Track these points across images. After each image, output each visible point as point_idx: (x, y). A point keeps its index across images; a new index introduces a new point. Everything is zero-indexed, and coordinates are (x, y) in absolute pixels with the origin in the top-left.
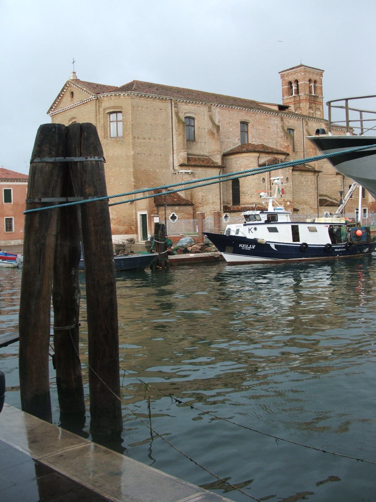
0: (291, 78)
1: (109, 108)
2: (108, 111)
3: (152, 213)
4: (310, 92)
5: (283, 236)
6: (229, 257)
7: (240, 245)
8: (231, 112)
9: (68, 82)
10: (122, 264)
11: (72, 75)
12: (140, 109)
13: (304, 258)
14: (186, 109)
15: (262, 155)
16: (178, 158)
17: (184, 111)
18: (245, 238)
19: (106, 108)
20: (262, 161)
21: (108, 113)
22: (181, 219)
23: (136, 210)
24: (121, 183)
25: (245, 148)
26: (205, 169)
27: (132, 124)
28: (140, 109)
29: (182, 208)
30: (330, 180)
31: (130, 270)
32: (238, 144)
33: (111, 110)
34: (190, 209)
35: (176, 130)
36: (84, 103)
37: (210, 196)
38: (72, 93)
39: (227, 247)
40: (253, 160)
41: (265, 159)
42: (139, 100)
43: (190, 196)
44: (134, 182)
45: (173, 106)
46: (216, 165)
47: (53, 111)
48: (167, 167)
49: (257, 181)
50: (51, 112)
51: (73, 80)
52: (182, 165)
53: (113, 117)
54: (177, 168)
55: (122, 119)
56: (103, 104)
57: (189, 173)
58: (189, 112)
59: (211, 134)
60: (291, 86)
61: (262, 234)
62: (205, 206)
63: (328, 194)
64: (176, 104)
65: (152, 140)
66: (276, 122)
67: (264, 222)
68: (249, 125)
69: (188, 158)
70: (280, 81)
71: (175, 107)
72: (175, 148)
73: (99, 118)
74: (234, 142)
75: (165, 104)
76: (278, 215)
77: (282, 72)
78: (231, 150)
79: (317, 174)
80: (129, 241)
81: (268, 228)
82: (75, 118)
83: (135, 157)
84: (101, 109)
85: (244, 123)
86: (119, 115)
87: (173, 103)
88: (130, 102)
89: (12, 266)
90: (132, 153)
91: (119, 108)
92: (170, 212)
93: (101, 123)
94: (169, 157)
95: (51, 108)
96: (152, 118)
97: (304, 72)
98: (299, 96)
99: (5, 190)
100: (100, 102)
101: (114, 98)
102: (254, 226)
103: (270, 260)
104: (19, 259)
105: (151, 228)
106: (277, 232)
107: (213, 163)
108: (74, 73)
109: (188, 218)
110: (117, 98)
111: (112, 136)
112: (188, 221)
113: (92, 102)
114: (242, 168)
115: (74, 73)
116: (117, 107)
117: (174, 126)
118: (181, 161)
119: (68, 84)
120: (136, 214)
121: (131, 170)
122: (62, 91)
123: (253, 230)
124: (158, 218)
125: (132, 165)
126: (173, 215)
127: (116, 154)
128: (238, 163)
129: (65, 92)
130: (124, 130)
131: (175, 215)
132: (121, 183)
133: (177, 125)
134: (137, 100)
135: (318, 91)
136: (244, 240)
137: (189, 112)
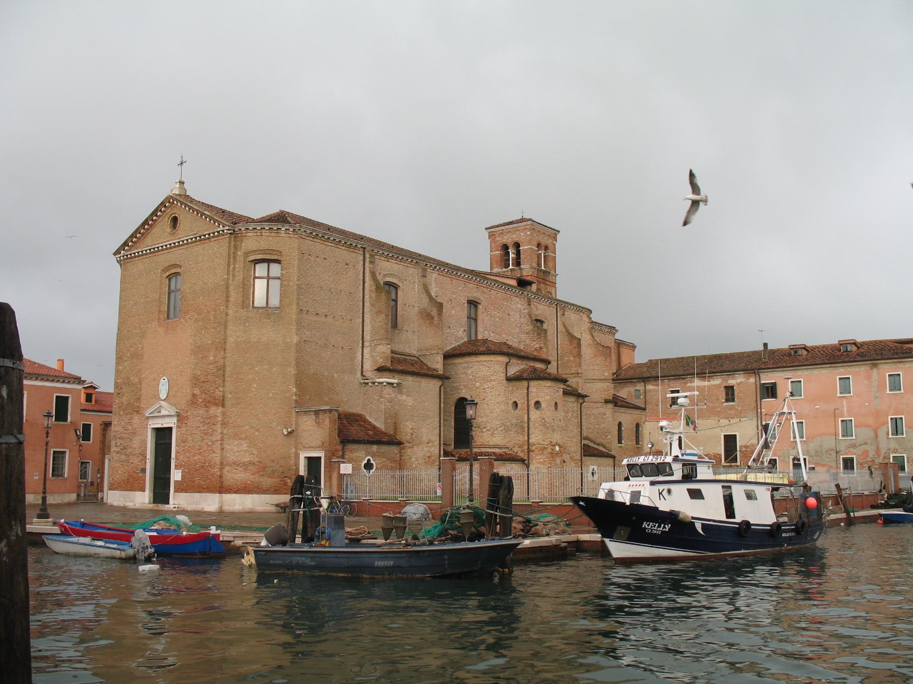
0: (509, 239)
3: (333, 454)
4: (539, 265)
5: (708, 509)
6: (618, 549)
7: (645, 525)
8: (454, 281)
9: (168, 199)
10: (446, 562)
11: (178, 185)
12: (313, 259)
13: (743, 551)
14: (388, 269)
15: (513, 361)
16: (372, 356)
17: (384, 273)
18: (656, 509)
20: (512, 371)
21: (252, 261)
22: (381, 469)
23: (297, 449)
24: (271, 395)
25: (474, 348)
26: (419, 379)
27: (298, 285)
28: (313, 259)
29: (384, 448)
30: (595, 411)
31: (459, 576)
32: (462, 338)
34: (394, 449)
35: (372, 305)
36: (201, 239)
37: (424, 430)
38: (175, 220)
39: (619, 528)
40: (497, 367)
41: (516, 367)
42: (311, 243)
43: (392, 428)
44: (296, 395)
45: (367, 260)
46: (435, 373)
47: (127, 251)
48: (352, 371)
49: (503, 407)
51: (180, 195)
52: (381, 370)
53: (261, 270)
54: (369, 374)
55: (279, 275)
57: (392, 384)
58: (391, 275)
59: (426, 316)
60: (507, 253)
61: (676, 501)
62: (415, 448)
63: (591, 436)
64: (372, 256)
65: (330, 319)
66: (519, 306)
67: (680, 479)
68: (480, 307)
69: (392, 357)
70: (487, 242)
71: (371, 262)
72: (367, 337)
73: (234, 268)
74: (457, 336)
75: (353, 255)
77: (492, 227)
78: (454, 349)
79: (581, 401)
80: (282, 508)
81: (689, 490)
82: (180, 266)
83: (301, 347)
84: (239, 253)
85: (473, 304)
86: (273, 266)
87: (367, 256)
88: (296, 244)
89: (123, 555)
90: (295, 339)
92: (363, 454)
93: (237, 278)
94: (356, 353)
95: (126, 244)
96: (331, 279)
97: (530, 230)
98: (521, 269)
99: (68, 397)
100: (239, 239)
102: (666, 487)
103: (691, 554)
104: (140, 540)
105: (331, 484)
106: (703, 498)
107: (429, 368)
108: (182, 183)
109: (392, 469)
111: (256, 305)
112: (391, 473)
113: (221, 237)
115: (182, 183)
117: (367, 297)
118: (381, 362)
119: (169, 202)
121: (292, 371)
122: (154, 213)
123: (665, 493)
124: (350, 466)
125: (294, 363)
126: (369, 460)
128: (469, 372)
129: (160, 216)
130: (283, 295)
131: (372, 462)
132: (271, 395)
133: (373, 295)
134: (309, 242)
135: (550, 264)
136: (652, 513)
137: (391, 275)
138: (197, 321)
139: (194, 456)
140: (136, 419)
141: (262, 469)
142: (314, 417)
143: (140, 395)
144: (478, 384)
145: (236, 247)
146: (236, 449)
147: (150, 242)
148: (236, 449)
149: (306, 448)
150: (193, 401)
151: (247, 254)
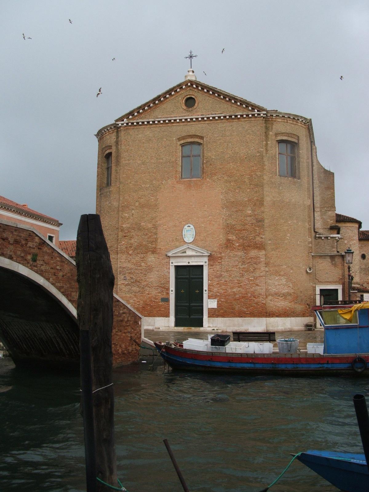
1: (282, 133)
2: (279, 138)
19: (280, 134)
33: (285, 138)
35: (320, 182)
50: (125, 120)
56: (274, 127)
76: (209, 307)
91: (294, 137)
95: (131, 113)
101: (291, 122)
110: (294, 123)
114: (346, 240)
116: (292, 136)
117: (316, 176)
120: (314, 290)
122: (169, 92)
127: (293, 200)
138: (226, 181)
139: (232, 288)
140: (151, 259)
141: (296, 299)
142: (329, 260)
143: (156, 239)
144: (346, 242)
145: (267, 128)
146: (277, 283)
147: (159, 115)
148: (277, 283)
149: (321, 282)
150: (229, 244)
151: (276, 135)
